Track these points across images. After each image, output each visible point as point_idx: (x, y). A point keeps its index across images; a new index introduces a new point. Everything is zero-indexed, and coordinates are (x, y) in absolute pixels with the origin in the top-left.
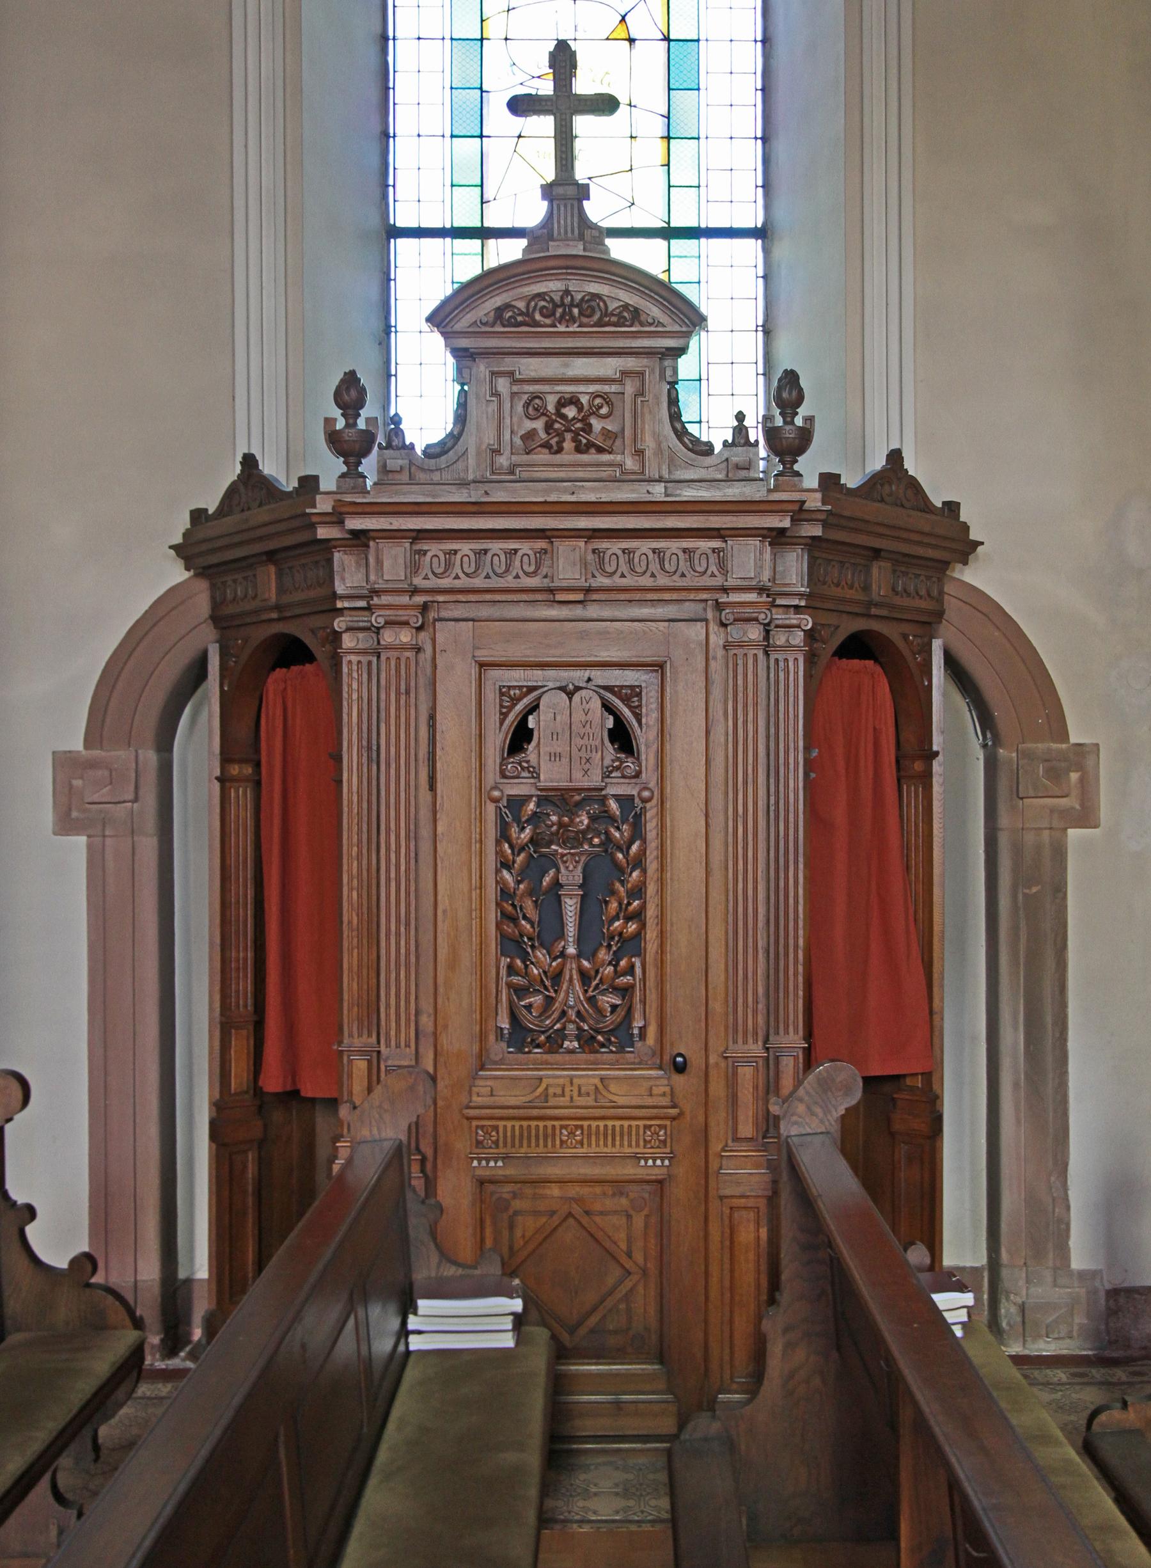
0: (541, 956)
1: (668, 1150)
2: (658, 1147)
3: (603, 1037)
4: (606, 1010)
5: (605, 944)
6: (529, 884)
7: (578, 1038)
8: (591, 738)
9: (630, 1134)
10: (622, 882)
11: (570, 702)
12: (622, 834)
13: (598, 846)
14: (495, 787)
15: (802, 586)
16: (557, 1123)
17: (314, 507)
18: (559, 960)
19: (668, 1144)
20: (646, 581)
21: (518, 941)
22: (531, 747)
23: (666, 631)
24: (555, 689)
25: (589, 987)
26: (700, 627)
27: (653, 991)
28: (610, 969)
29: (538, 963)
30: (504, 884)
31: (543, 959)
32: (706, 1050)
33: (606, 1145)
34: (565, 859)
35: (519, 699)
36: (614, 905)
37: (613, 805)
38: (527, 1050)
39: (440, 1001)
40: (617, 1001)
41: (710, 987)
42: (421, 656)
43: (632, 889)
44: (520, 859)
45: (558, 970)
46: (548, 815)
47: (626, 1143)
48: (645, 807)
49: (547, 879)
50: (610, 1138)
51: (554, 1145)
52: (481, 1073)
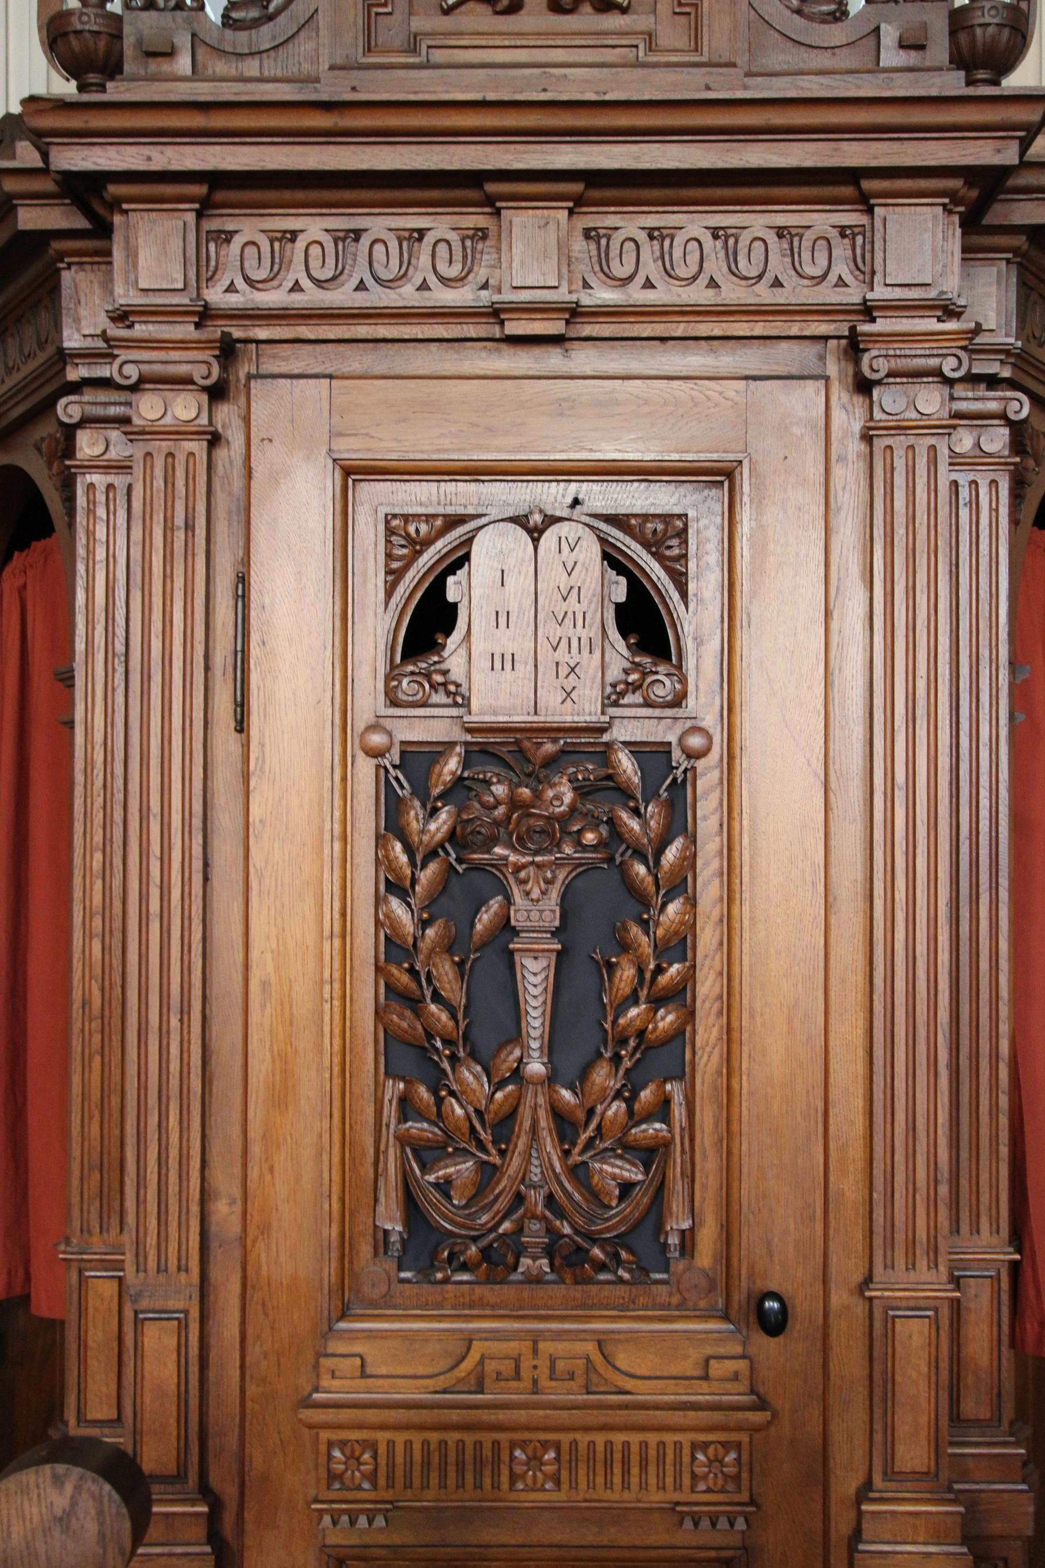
0: (471, 1079)
1: (744, 1497)
2: (722, 1491)
3: (603, 1249)
4: (608, 1194)
5: (608, 1055)
6: (446, 927)
7: (550, 1252)
8: (580, 623)
9: (661, 1460)
10: (645, 925)
11: (536, 549)
12: (645, 824)
13: (594, 848)
14: (374, 727)
15: (1007, 335)
16: (503, 1437)
17: (13, 157)
18: (510, 1088)
19: (745, 1483)
20: (698, 295)
21: (423, 1048)
22: (453, 640)
23: (741, 400)
24: (503, 520)
25: (574, 1144)
26: (811, 393)
27: (711, 1153)
28: (618, 1107)
29: (463, 1093)
30: (392, 927)
31: (474, 1085)
32: (825, 1282)
33: (609, 1485)
34: (523, 874)
35: (428, 543)
36: (626, 973)
37: (626, 764)
38: (439, 1276)
39: (254, 1173)
40: (636, 1175)
41: (832, 1145)
42: (221, 454)
43: (666, 940)
44: (427, 875)
45: (506, 1109)
46: (488, 783)
47: (652, 1480)
48: (694, 768)
49: (485, 917)
50: (617, 1470)
51: (496, 1486)
52: (342, 1325)
